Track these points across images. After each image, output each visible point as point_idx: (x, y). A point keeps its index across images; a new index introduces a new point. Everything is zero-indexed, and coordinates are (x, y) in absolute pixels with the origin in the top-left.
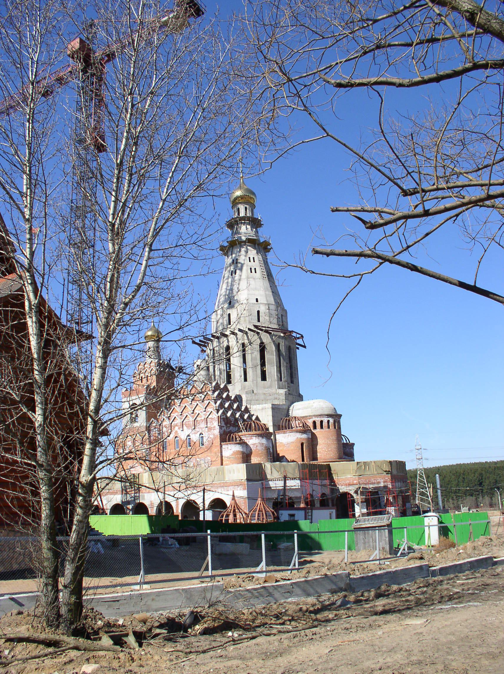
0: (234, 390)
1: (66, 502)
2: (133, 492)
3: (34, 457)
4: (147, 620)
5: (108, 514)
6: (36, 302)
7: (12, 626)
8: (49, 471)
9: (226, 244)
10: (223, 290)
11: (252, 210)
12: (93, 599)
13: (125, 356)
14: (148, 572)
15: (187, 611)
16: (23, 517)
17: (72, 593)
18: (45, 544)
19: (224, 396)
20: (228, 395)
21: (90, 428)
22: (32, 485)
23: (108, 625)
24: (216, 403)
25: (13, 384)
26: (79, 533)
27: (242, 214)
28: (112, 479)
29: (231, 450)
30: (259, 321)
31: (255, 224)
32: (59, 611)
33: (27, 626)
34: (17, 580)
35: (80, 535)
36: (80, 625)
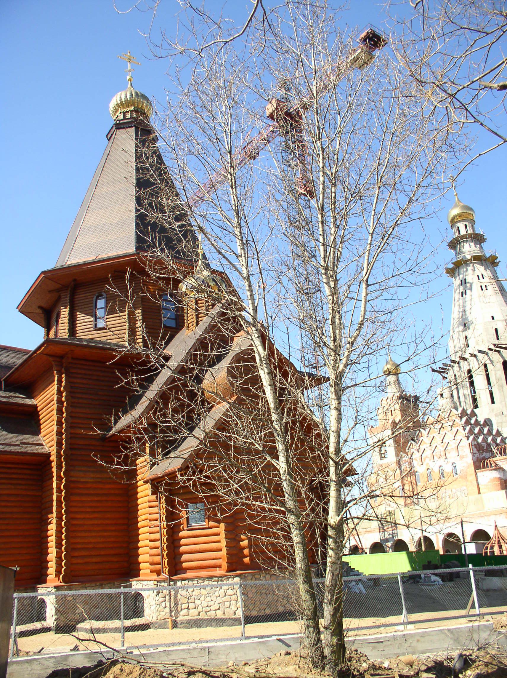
0: (482, 414)
1: (316, 545)
2: (391, 529)
3: (283, 504)
4: (413, 663)
5: (368, 552)
6: (266, 353)
7: (281, 665)
8: (298, 517)
9: (451, 266)
10: (456, 314)
11: (472, 226)
12: (355, 640)
13: (358, 393)
14: (410, 611)
15: (455, 654)
16: (278, 562)
17: (333, 634)
18: (303, 588)
19: (473, 421)
20: (476, 420)
21: (332, 469)
22: (283, 529)
23: (374, 667)
24: (464, 430)
25: (254, 435)
26: (333, 574)
27: (463, 232)
28: (361, 519)
29: (488, 476)
30: (498, 339)
31: (478, 240)
32: (322, 652)
33: (295, 666)
34: (285, 622)
35: (334, 577)
36: (345, 667)
